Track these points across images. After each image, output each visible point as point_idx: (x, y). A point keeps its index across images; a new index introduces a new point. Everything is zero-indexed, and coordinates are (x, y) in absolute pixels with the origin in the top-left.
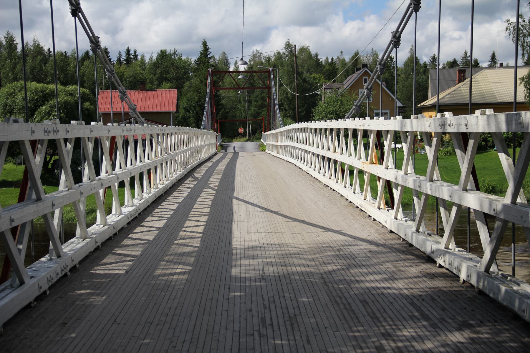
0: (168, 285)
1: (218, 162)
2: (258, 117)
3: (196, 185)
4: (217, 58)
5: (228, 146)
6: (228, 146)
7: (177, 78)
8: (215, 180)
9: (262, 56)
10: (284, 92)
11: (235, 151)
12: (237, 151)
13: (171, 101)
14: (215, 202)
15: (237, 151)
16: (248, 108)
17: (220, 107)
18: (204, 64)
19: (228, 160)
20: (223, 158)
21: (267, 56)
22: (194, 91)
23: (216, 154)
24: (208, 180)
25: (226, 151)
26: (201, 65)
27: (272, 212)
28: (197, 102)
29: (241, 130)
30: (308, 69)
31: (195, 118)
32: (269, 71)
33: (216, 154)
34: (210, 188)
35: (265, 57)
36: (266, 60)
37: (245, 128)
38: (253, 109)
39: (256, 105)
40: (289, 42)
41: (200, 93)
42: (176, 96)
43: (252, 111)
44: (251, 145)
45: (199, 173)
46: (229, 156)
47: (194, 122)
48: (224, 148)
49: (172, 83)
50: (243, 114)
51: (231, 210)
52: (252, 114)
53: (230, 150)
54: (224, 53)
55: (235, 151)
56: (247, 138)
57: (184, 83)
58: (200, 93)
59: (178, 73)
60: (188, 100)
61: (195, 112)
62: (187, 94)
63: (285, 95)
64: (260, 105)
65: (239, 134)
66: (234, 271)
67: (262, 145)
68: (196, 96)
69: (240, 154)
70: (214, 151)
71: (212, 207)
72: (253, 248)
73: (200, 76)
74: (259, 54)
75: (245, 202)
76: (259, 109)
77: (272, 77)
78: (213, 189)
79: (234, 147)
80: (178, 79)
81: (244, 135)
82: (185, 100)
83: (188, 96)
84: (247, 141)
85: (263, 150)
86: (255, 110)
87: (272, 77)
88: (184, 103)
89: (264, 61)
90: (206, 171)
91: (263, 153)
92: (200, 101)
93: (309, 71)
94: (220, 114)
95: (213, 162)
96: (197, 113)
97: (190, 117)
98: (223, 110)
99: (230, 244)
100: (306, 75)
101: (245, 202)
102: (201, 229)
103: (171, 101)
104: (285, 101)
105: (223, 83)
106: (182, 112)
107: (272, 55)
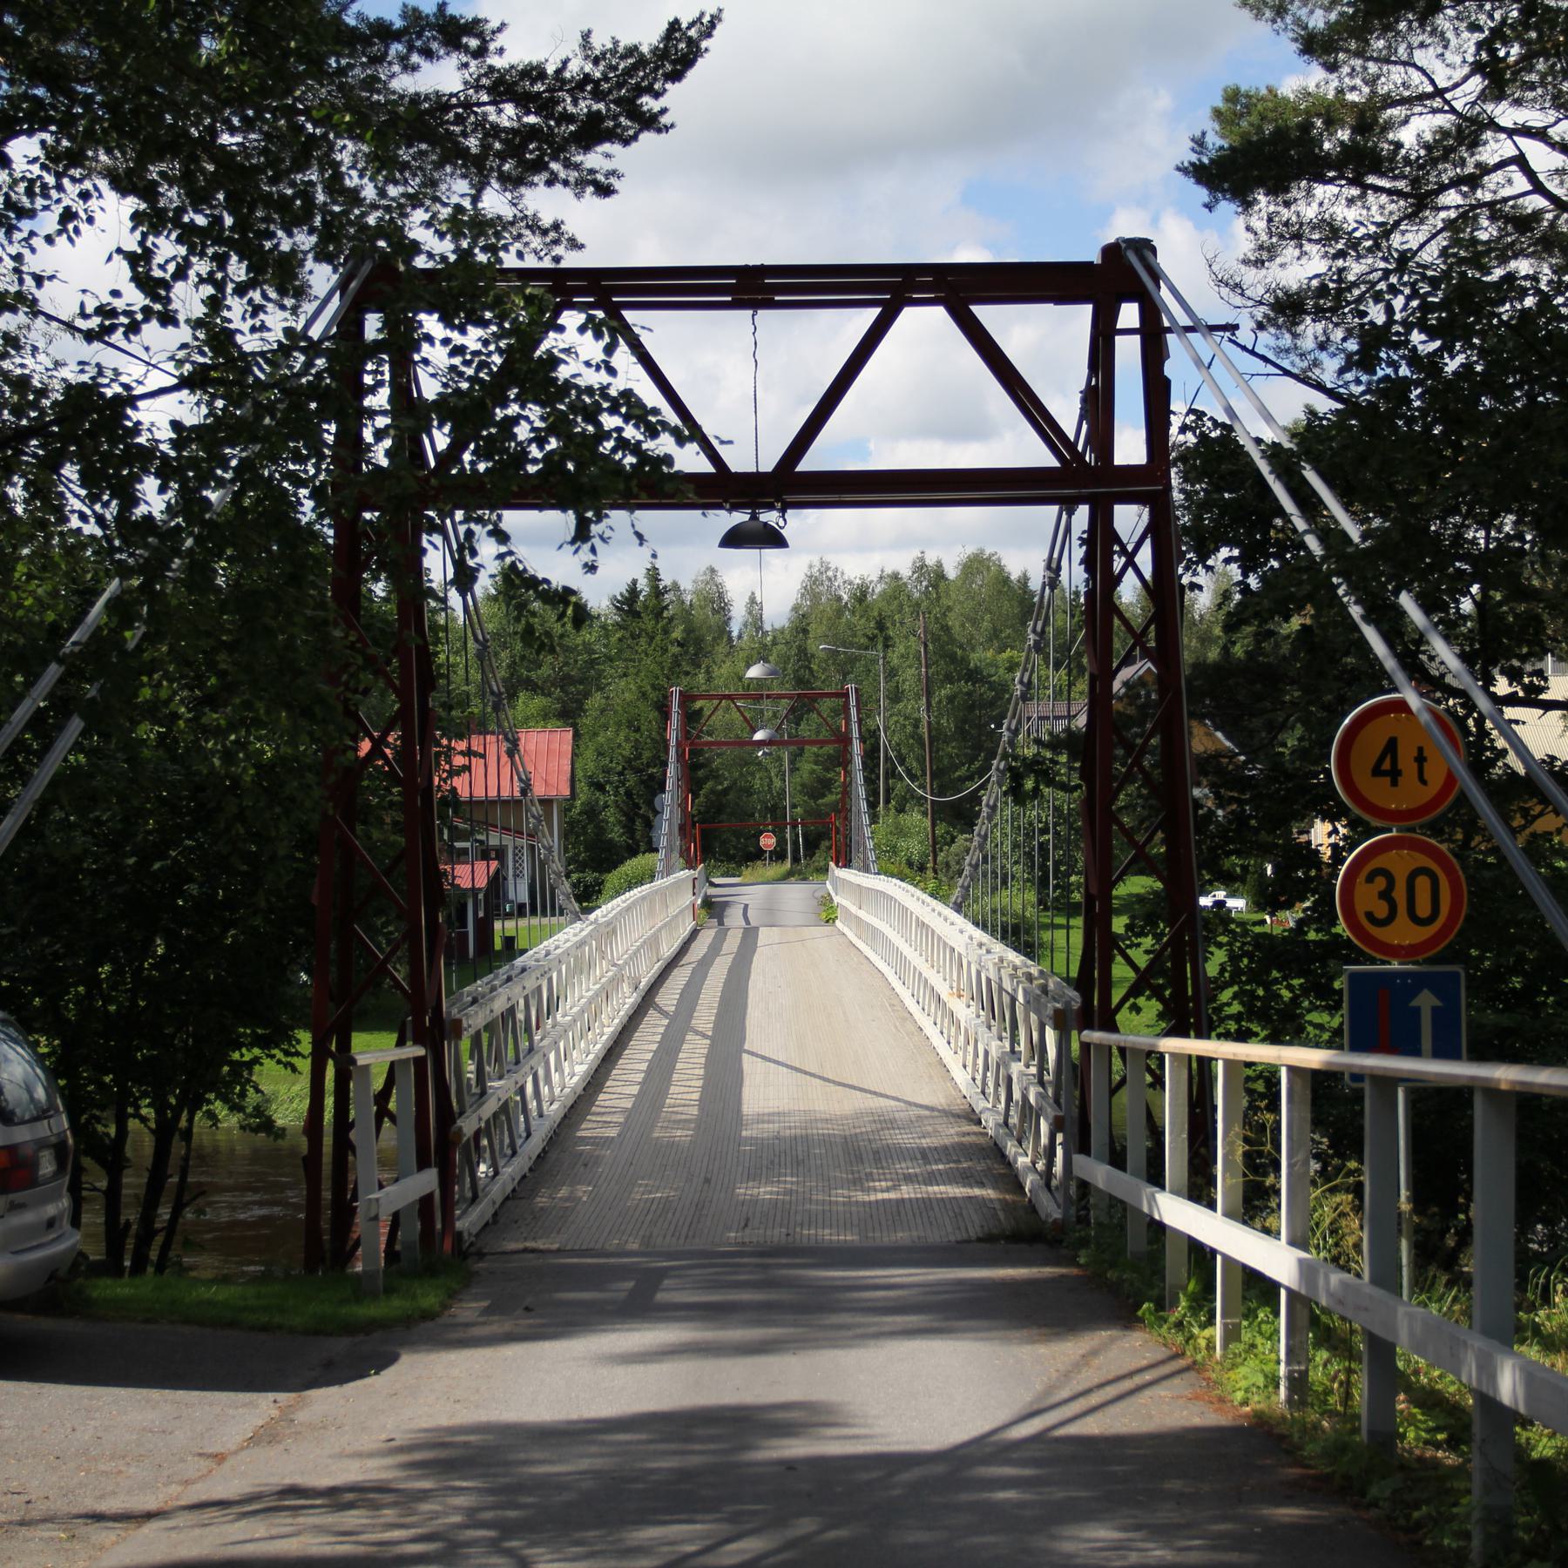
0: (672, 1145)
1: (705, 964)
2: (823, 796)
3: (668, 1027)
4: (686, 584)
5: (726, 904)
6: (726, 904)
7: (562, 679)
8: (705, 1017)
9: (839, 582)
10: (907, 718)
11: (747, 922)
12: (753, 923)
13: (554, 766)
14: (710, 1058)
15: (753, 923)
16: (792, 762)
17: (701, 773)
18: (652, 638)
19: (730, 959)
20: (715, 950)
21: (858, 581)
22: (619, 724)
23: (694, 934)
24: (691, 1017)
25: (721, 923)
26: (643, 641)
27: (806, 1073)
28: (629, 761)
29: (768, 842)
30: (995, 630)
31: (621, 810)
32: (846, 695)
33: (694, 934)
34: (697, 1033)
35: (851, 583)
36: (853, 596)
37: (779, 832)
38: (807, 767)
39: (817, 756)
40: (922, 559)
41: (638, 730)
42: (568, 748)
43: (806, 775)
44: (795, 895)
45: (668, 997)
46: (732, 942)
47: (620, 822)
48: (713, 908)
49: (549, 695)
50: (777, 783)
51: (740, 1071)
52: (803, 785)
53: (734, 918)
54: (713, 571)
55: (747, 922)
56: (788, 864)
57: (587, 695)
58: (638, 730)
59: (566, 664)
60: (600, 754)
61: (622, 790)
62: (596, 734)
63: (909, 729)
64: (830, 757)
65: (758, 855)
66: (744, 1133)
67: (826, 903)
68: (627, 739)
69: (763, 932)
70: (689, 925)
71: (706, 1066)
72: (773, 1114)
73: (637, 674)
74: (830, 574)
75: (764, 1058)
76: (827, 770)
77: (853, 711)
78: (704, 1036)
79: (746, 906)
80: (564, 681)
81: (778, 855)
82: (589, 754)
83: (601, 739)
84: (785, 878)
85: (830, 921)
86: (812, 772)
87: (853, 711)
88: (589, 763)
89: (845, 597)
90: (681, 995)
91: (827, 929)
92: (639, 757)
93: (997, 637)
94: (702, 799)
95: (690, 968)
96: (629, 794)
97: (606, 806)
98: (709, 785)
99: (739, 1110)
100: (980, 656)
101: (764, 1058)
102: (696, 1096)
103: (554, 766)
104: (911, 748)
105: (709, 679)
106: (585, 792)
107: (875, 578)
